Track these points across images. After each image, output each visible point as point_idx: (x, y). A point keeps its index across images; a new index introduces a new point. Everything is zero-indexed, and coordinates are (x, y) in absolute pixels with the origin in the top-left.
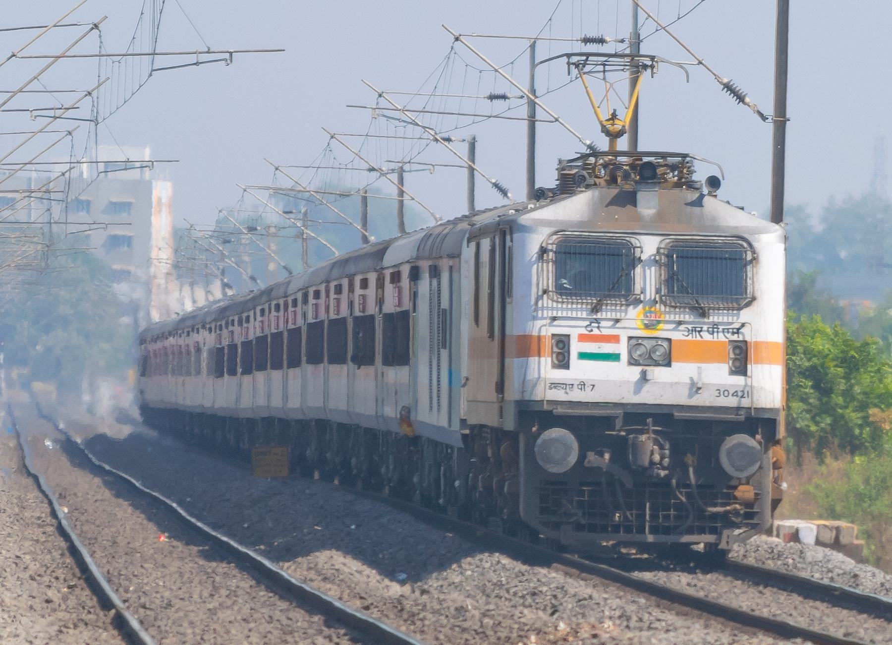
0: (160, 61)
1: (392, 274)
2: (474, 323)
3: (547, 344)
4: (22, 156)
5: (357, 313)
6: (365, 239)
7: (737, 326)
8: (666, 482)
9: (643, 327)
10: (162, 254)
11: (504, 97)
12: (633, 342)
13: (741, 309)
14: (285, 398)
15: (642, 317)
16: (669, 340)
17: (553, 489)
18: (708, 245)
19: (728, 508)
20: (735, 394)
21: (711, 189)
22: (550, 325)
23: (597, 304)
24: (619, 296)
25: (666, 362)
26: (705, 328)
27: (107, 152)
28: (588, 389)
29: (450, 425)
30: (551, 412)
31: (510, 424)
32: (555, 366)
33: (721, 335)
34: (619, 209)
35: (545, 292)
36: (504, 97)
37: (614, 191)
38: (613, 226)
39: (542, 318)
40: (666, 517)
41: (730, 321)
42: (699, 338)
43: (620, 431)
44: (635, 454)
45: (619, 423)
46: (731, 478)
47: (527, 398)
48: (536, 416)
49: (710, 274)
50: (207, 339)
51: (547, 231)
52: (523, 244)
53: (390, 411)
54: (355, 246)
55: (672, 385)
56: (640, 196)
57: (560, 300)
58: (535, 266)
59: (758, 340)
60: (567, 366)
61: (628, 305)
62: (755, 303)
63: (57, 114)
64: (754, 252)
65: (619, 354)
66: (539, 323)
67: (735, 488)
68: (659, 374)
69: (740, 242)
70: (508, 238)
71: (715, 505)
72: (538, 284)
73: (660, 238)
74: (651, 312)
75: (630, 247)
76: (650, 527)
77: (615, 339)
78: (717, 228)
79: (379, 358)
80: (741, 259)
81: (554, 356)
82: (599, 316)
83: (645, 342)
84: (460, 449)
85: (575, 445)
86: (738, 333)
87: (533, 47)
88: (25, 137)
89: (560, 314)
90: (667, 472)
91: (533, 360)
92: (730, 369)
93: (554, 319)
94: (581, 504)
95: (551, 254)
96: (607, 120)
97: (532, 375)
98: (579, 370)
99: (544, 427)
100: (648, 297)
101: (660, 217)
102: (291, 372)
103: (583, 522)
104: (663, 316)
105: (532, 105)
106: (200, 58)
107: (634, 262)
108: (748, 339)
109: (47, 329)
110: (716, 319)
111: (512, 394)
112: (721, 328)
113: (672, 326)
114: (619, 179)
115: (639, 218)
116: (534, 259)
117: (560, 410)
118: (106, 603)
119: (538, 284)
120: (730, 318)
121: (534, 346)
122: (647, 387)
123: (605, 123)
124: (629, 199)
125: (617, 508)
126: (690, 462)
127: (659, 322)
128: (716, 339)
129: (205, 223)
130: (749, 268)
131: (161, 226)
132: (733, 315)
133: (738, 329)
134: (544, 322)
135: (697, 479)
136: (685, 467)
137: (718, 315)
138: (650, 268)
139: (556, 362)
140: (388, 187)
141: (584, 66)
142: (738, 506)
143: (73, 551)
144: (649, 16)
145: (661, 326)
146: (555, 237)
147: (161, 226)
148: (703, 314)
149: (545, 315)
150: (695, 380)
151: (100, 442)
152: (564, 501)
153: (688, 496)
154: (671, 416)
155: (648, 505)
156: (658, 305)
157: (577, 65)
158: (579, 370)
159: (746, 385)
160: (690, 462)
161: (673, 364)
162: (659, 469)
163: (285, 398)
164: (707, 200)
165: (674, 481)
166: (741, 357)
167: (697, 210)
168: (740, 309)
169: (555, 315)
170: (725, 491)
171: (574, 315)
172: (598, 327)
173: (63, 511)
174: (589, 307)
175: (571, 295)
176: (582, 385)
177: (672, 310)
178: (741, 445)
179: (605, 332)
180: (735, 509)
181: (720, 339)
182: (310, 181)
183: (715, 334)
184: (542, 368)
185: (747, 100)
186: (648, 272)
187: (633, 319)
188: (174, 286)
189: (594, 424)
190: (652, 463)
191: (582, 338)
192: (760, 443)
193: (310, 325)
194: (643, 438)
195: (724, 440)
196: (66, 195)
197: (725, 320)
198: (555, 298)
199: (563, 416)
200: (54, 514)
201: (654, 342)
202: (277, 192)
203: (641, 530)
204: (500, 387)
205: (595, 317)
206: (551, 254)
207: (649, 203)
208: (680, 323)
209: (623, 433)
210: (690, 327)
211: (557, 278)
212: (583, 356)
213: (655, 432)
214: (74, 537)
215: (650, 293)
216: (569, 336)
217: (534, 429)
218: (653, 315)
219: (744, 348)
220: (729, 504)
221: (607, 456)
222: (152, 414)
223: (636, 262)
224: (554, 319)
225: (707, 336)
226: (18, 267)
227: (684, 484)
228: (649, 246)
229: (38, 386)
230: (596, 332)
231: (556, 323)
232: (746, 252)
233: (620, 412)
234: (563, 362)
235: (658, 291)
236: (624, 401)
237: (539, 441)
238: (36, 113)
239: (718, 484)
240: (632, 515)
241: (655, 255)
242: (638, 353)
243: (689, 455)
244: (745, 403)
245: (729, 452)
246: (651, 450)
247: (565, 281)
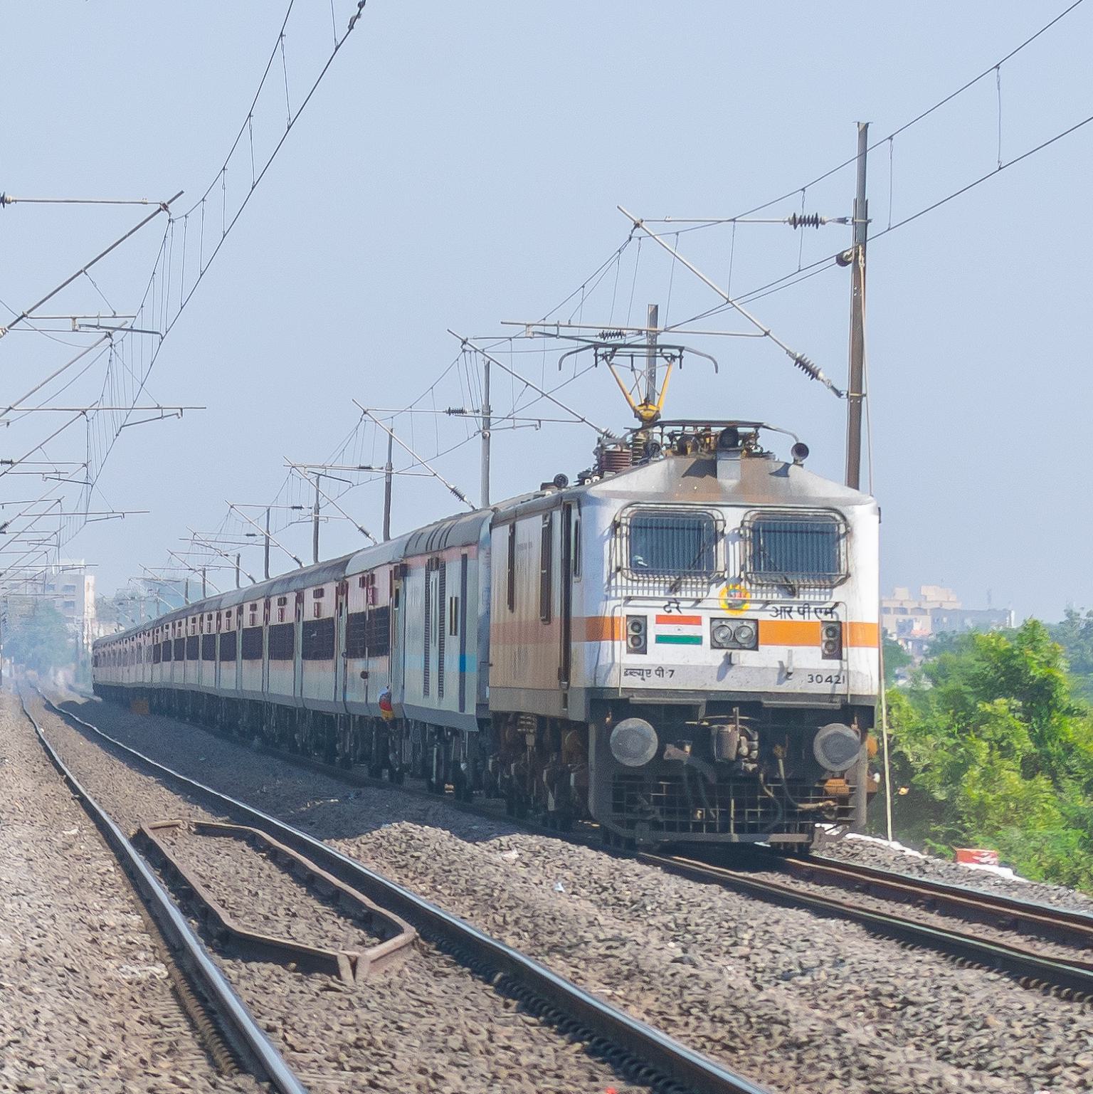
0: (90, 517)
1: (280, 600)
2: (508, 607)
3: (622, 627)
4: (21, 564)
5: (190, 635)
6: (187, 602)
7: (830, 605)
8: (752, 777)
9: (727, 607)
10: (90, 611)
11: (254, 535)
12: (716, 623)
13: (835, 587)
14: (144, 677)
15: (725, 596)
16: (756, 621)
17: (627, 786)
18: (796, 517)
19: (821, 804)
20: (829, 679)
21: (797, 458)
22: (625, 605)
23: (676, 583)
24: (700, 574)
25: (751, 645)
26: (795, 608)
27: (64, 562)
28: (667, 675)
29: (462, 707)
30: (627, 700)
31: (577, 712)
32: (630, 651)
33: (813, 615)
34: (698, 480)
35: (618, 569)
36: (254, 535)
37: (689, 461)
38: (693, 499)
39: (616, 598)
40: (753, 814)
41: (823, 599)
42: (788, 619)
43: (702, 721)
44: (720, 745)
45: (702, 713)
46: (824, 770)
47: (600, 684)
48: (610, 705)
49: (800, 549)
50: (148, 641)
51: (620, 503)
52: (594, 519)
53: (375, 698)
54: (182, 605)
55: (759, 669)
56: (720, 465)
57: (635, 578)
58: (608, 542)
59: (854, 620)
60: (644, 651)
61: (710, 584)
62: (849, 580)
63: (41, 542)
64: (847, 525)
65: (645, 652)
66: (612, 604)
67: (825, 781)
68: (745, 658)
69: (833, 514)
70: (574, 512)
71: (807, 801)
72: (610, 561)
73: (744, 510)
74: (735, 591)
75: (712, 520)
76: (736, 825)
77: (697, 621)
78: (805, 499)
79: (239, 655)
80: (833, 532)
81: (630, 639)
82: (678, 595)
83: (729, 624)
84: (471, 733)
85: (654, 737)
86: (831, 612)
87: (268, 510)
88: (30, 529)
89: (635, 594)
90: (755, 765)
91: (606, 644)
92: (823, 653)
93: (629, 599)
94: (658, 801)
95: (625, 529)
96: (642, 405)
97: (605, 660)
99: (619, 717)
100: (732, 575)
101: (743, 488)
102: (224, 664)
103: (661, 820)
104: (749, 595)
105: (268, 539)
106: (110, 515)
107: (716, 536)
108: (842, 619)
109: (34, 646)
110: (807, 598)
111: (581, 678)
112: (812, 608)
113: (759, 606)
114: (689, 450)
115: (719, 489)
116: (606, 533)
117: (636, 699)
118: (62, 772)
119: (610, 561)
120: (823, 597)
121: (607, 628)
122: (731, 672)
123: (638, 408)
124: (707, 468)
125: (699, 804)
126: (780, 754)
127: (745, 602)
128: (807, 619)
129: (110, 596)
130: (842, 542)
131: (90, 597)
132: (826, 594)
133: (832, 609)
134: (618, 602)
135: (786, 771)
136: (773, 760)
137: (809, 593)
138: (733, 543)
139: (631, 646)
140: (198, 578)
141: (612, 358)
142: (831, 803)
143: (47, 750)
144: (528, 384)
145: (747, 606)
146: (629, 509)
147: (90, 597)
148: (793, 593)
149: (619, 595)
150: (785, 664)
151: (70, 705)
152: (640, 798)
153: (776, 791)
154: (760, 703)
155: (733, 801)
156: (743, 583)
157: (604, 357)
158: (657, 655)
159: (841, 669)
160: (780, 754)
161: (760, 647)
162: (746, 762)
163: (144, 677)
164: (792, 469)
165: (762, 776)
166: (835, 640)
167: (783, 479)
168: (833, 587)
169: (630, 594)
170: (817, 785)
171: (651, 595)
172: (677, 608)
173: (41, 731)
174: (667, 586)
175: (647, 573)
176: (660, 671)
177: (759, 588)
178: (838, 735)
179: (685, 613)
180: (828, 805)
181: (811, 620)
182: (163, 576)
183: (806, 614)
184: (617, 653)
185: (821, 375)
186: (731, 547)
187: (716, 599)
188: (96, 624)
189: (671, 714)
190: (739, 756)
191: (660, 620)
192: (857, 733)
193: (245, 631)
194: (729, 728)
195: (818, 731)
196: (43, 581)
197: (817, 599)
198: (630, 576)
199: (781, 709)
200: (37, 732)
201: (739, 624)
202: (147, 581)
203: (726, 829)
204: (565, 672)
205: (673, 596)
206: (625, 529)
207: (730, 472)
208: (767, 603)
209: (706, 723)
210: (778, 606)
211: (632, 553)
212: (661, 639)
213: (742, 722)
214: (47, 743)
215: (734, 571)
216: (646, 617)
217: (608, 719)
218: (738, 594)
219: (838, 629)
220: (821, 801)
221: (688, 748)
222: (99, 689)
223: (719, 536)
224: (629, 599)
225: (796, 617)
226: (21, 616)
227: (771, 779)
228: (732, 518)
229: (29, 672)
230: (675, 612)
231: (631, 603)
232: (838, 525)
233: (702, 700)
234: (639, 646)
235: (743, 568)
236: (707, 688)
237: (614, 733)
238: (30, 543)
239: (807, 777)
240: (715, 812)
241: (739, 529)
242: (722, 635)
243: (779, 747)
244: (840, 689)
245: (824, 744)
246: (738, 741)
247: (640, 558)
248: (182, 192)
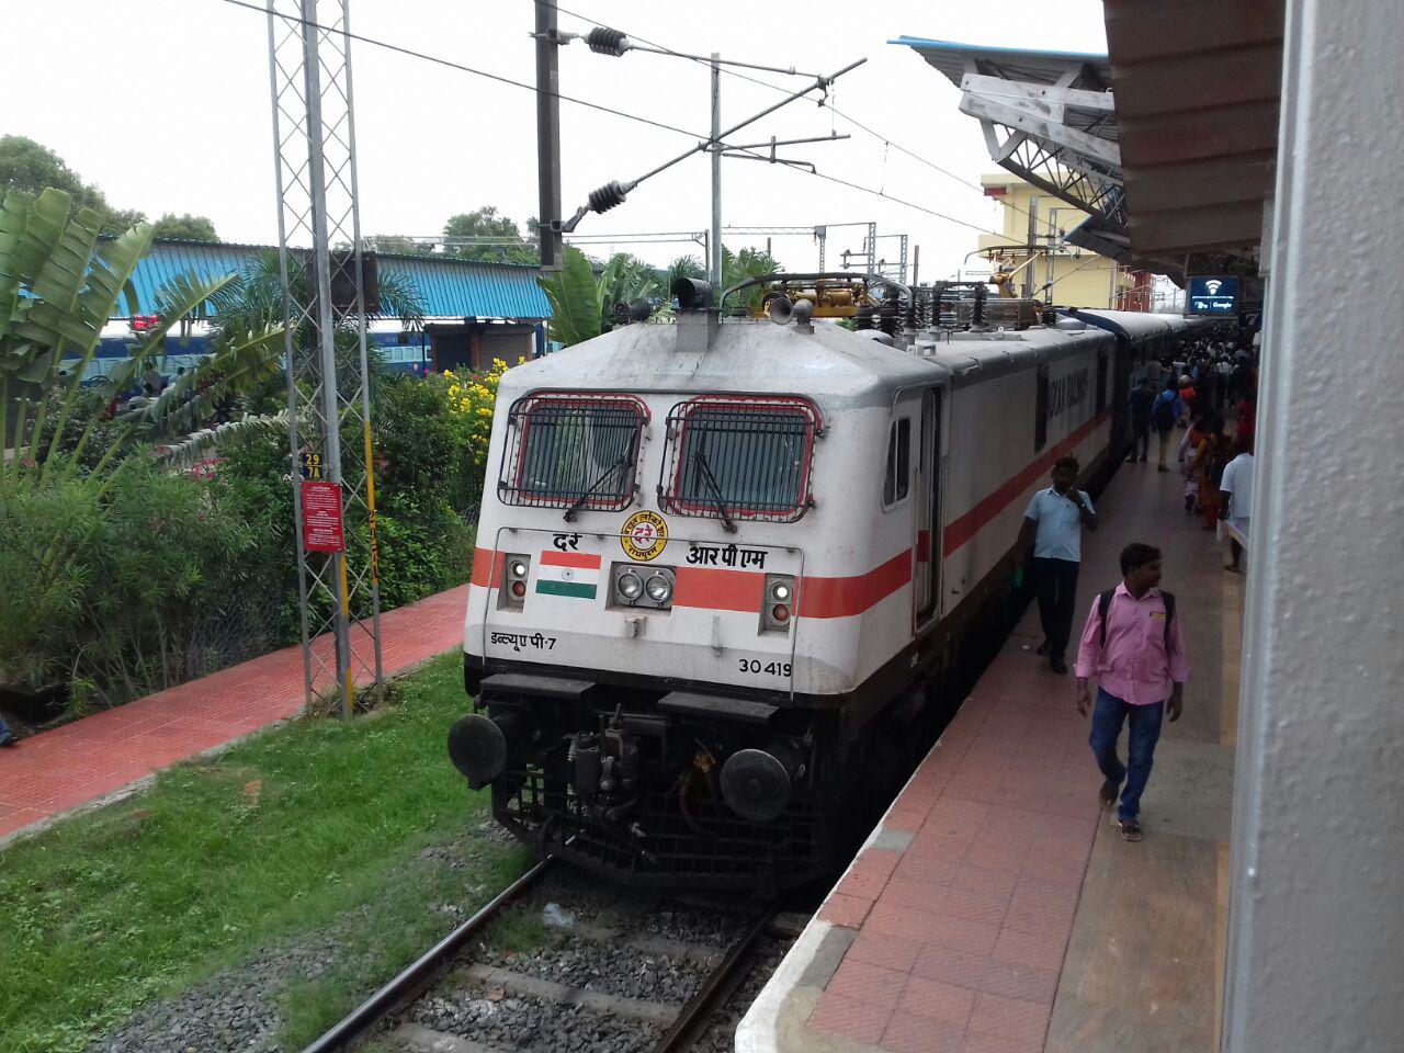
14: (319, 228)
60: (519, 606)
65: (538, 591)
68: (658, 624)
77: (592, 562)
98: (540, 613)
163: (319, 228)
176: (538, 639)
191: (548, 559)
212: (545, 587)
248: (889, 42)
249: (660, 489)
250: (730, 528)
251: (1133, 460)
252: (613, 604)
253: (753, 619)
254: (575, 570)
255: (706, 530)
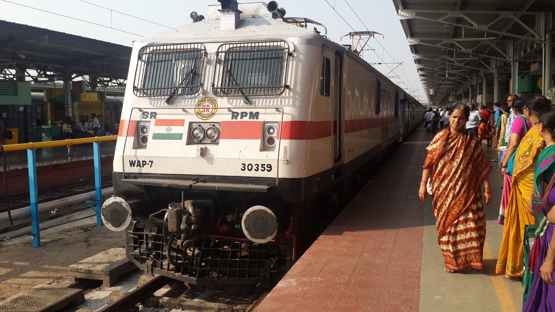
212: (157, 136)
249: (213, 85)
250: (248, 101)
251: (529, 211)
252: (190, 141)
253: (257, 143)
254: (173, 127)
255: (238, 104)
